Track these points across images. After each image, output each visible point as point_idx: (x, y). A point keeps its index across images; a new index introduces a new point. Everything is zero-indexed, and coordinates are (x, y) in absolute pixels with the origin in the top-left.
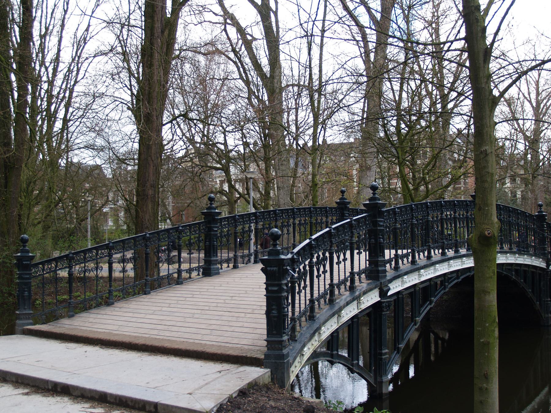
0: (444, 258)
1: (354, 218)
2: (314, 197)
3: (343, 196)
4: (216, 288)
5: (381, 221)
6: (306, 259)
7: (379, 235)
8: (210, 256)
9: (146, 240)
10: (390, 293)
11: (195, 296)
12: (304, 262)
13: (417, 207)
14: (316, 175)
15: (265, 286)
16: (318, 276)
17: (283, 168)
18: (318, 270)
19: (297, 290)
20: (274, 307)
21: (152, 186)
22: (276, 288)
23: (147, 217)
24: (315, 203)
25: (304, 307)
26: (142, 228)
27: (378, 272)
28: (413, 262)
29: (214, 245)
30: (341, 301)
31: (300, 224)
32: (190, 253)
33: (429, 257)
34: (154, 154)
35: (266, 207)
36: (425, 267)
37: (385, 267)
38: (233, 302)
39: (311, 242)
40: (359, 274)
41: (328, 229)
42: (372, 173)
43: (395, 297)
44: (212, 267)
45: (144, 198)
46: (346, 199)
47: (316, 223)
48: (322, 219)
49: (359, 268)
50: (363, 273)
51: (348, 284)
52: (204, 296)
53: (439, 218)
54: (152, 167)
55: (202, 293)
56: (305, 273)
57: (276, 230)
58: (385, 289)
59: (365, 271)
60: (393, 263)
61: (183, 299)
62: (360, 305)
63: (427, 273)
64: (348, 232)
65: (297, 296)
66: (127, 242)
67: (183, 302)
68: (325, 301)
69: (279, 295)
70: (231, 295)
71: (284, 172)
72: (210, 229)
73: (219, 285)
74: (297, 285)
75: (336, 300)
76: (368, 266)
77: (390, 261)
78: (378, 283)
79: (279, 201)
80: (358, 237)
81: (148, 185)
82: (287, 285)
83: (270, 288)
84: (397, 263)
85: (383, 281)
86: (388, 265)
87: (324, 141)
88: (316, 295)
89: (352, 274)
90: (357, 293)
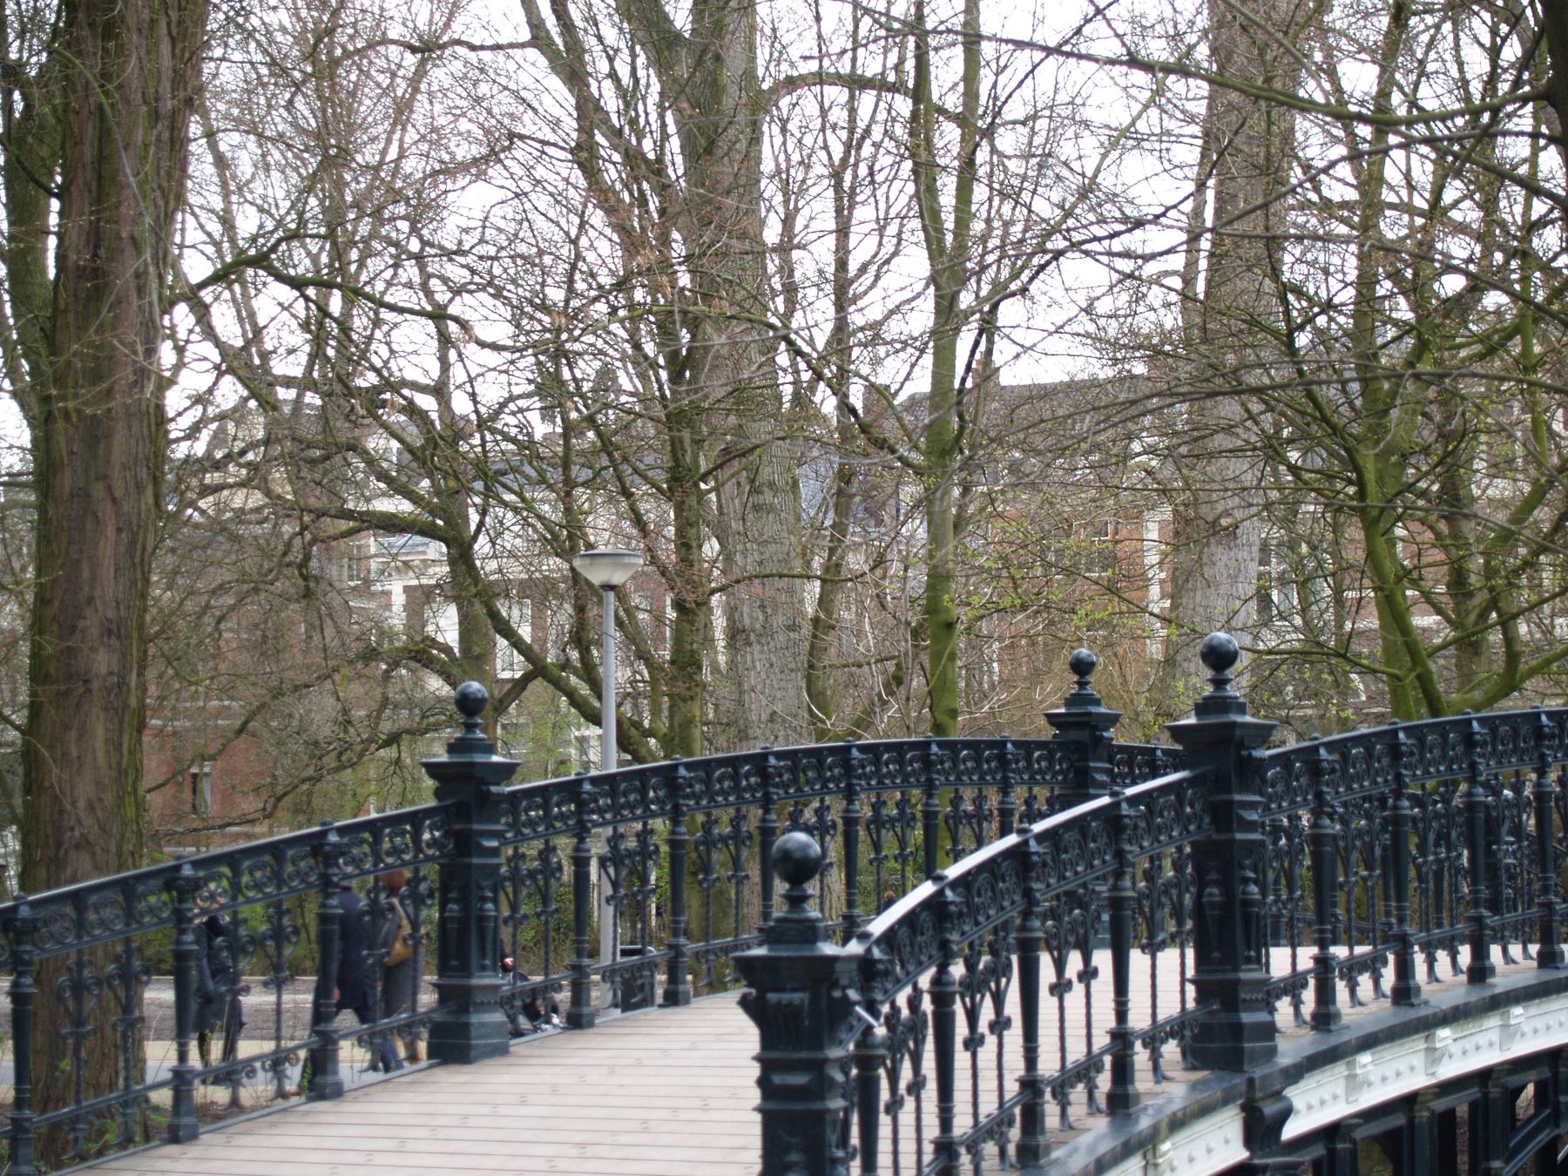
0: (1549, 975)
1: (1130, 791)
2: (938, 691)
4: (502, 1110)
5: (1252, 806)
6: (921, 967)
7: (1242, 867)
8: (465, 970)
10: (1290, 1131)
11: (410, 1146)
12: (911, 978)
13: (1421, 741)
14: (948, 577)
15: (755, 1070)
16: (973, 1043)
18: (972, 1016)
19: (885, 1095)
20: (794, 1157)
21: (112, 630)
22: (800, 1079)
23: (84, 789)
26: (59, 845)
27: (1237, 1030)
28: (1404, 993)
29: (482, 919)
31: (877, 822)
33: (1479, 972)
36: (1456, 1016)
40: (1153, 1040)
41: (1012, 839)
43: (1318, 1151)
45: (67, 694)
46: (1097, 702)
47: (956, 818)
48: (979, 800)
49: (1154, 1015)
50: (1172, 1035)
51: (1104, 1082)
52: (453, 1146)
53: (1528, 791)
54: (110, 531)
55: (442, 1134)
56: (916, 1027)
58: (1269, 1109)
59: (1176, 1028)
60: (1309, 996)
63: (1468, 1044)
64: (1099, 852)
65: (884, 1120)
66: (93, 899)
68: (1003, 1153)
69: (817, 1106)
70: (580, 1138)
71: (772, 548)
72: (464, 844)
73: (472, 1122)
74: (882, 1072)
75: (1048, 1149)
76: (1191, 1005)
77: (1293, 985)
78: (1239, 1081)
79: (741, 703)
80: (1150, 876)
81: (91, 623)
82: (844, 1066)
83: (777, 1079)
84: (1325, 995)
85: (1258, 1072)
86: (1284, 1006)
87: (986, 371)
88: (962, 1124)
89: (1121, 1038)
90: (1144, 1123)
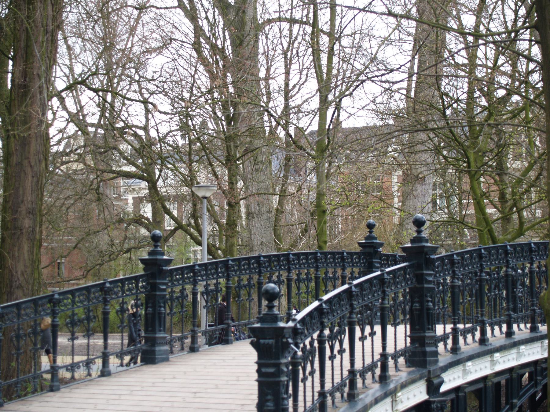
0: (534, 335)
2: (320, 234)
3: (371, 232)
5: (430, 275)
6: (314, 331)
7: (426, 296)
8: (154, 331)
9: (54, 304)
10: (443, 389)
11: (134, 393)
12: (311, 335)
14: (324, 194)
15: (256, 367)
16: (332, 358)
17: (261, 177)
18: (332, 348)
19: (301, 376)
20: (269, 397)
21: (30, 212)
22: (271, 370)
23: (20, 267)
24: (322, 244)
25: (311, 403)
26: (11, 287)
27: (425, 354)
28: (483, 341)
29: (160, 313)
30: (366, 397)
31: (299, 280)
32: (73, 339)
33: (509, 334)
34: (35, 155)
35: (228, 251)
37: (437, 347)
38: (197, 400)
39: (321, 305)
40: (395, 357)
42: (427, 187)
43: (453, 396)
44: (157, 348)
46: (376, 239)
47: (326, 279)
49: (395, 348)
50: (402, 355)
51: (378, 371)
52: (149, 393)
53: (527, 270)
54: (30, 177)
56: (312, 352)
57: (272, 285)
58: (436, 381)
59: (403, 353)
60: (450, 342)
61: (117, 397)
62: (397, 405)
63: (505, 359)
64: (377, 291)
65: (301, 385)
66: (23, 306)
67: (116, 402)
68: (342, 396)
69: (277, 379)
71: (262, 184)
74: (300, 368)
75: (358, 395)
76: (408, 344)
77: (444, 338)
78: (425, 371)
79: (251, 238)
80: (394, 299)
81: (23, 209)
82: (287, 365)
83: (264, 370)
84: (455, 341)
85: (432, 368)
86: (441, 345)
87: (337, 122)
88: (328, 386)
89: (384, 356)
90: (392, 386)
